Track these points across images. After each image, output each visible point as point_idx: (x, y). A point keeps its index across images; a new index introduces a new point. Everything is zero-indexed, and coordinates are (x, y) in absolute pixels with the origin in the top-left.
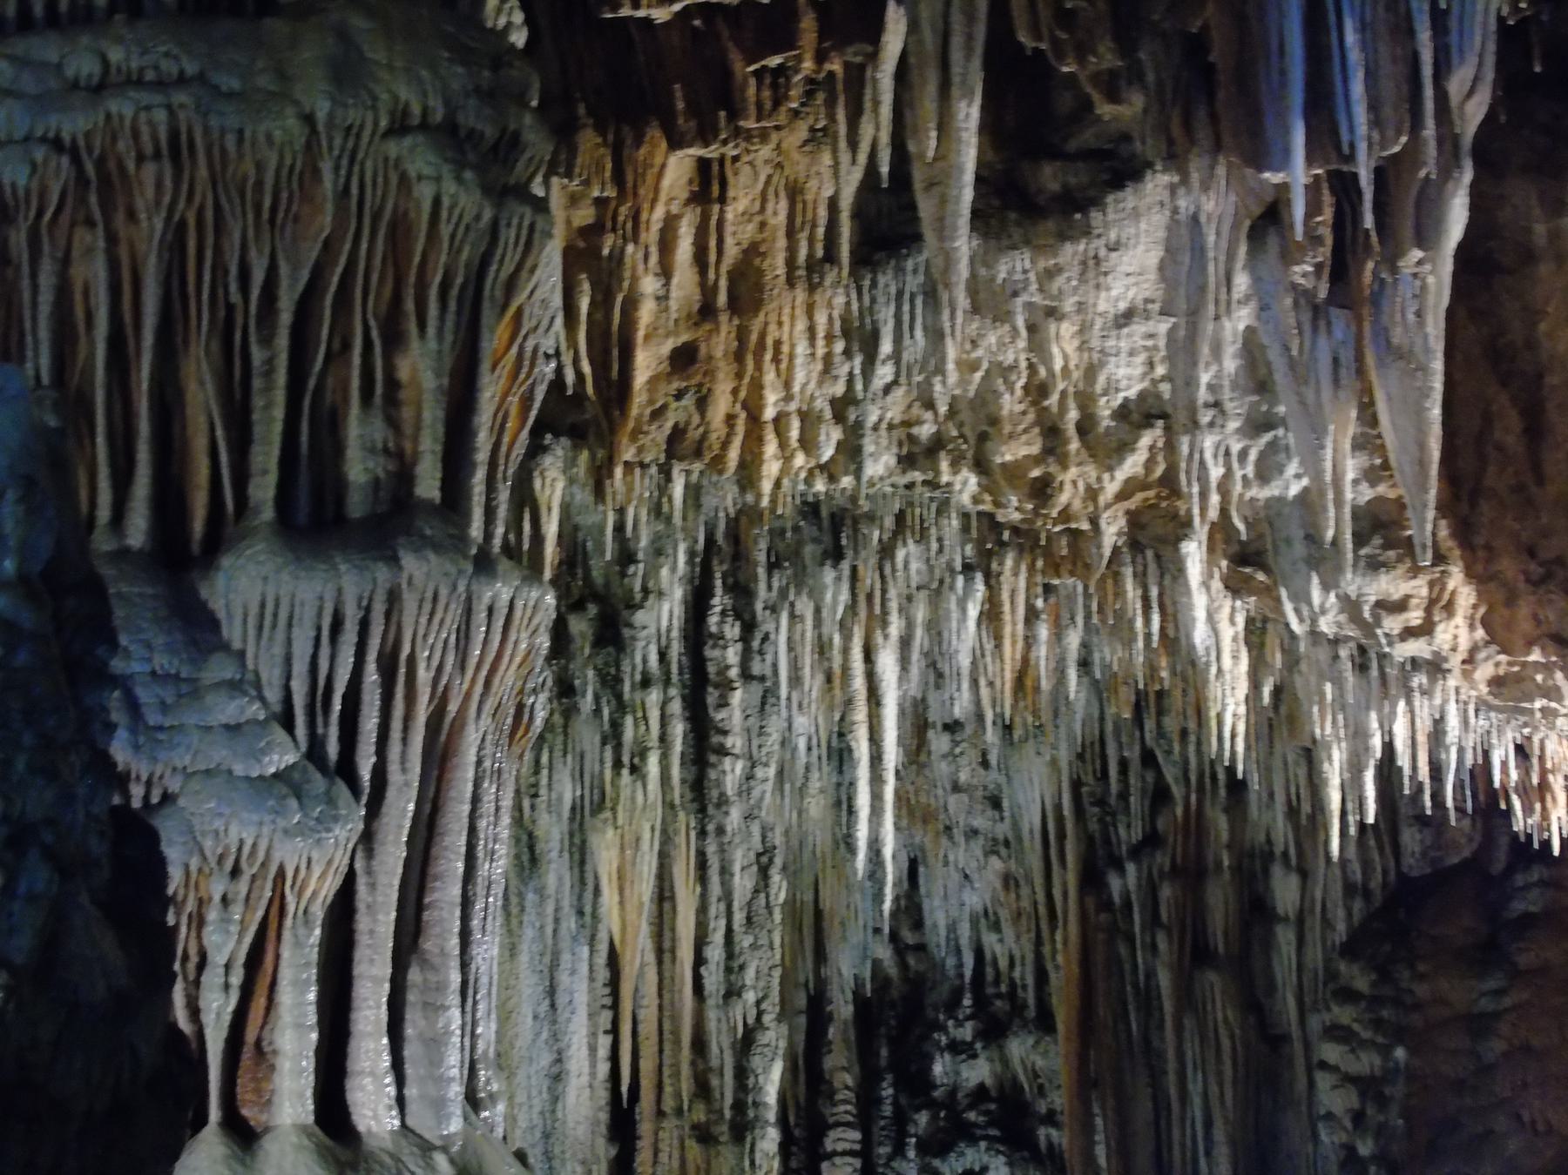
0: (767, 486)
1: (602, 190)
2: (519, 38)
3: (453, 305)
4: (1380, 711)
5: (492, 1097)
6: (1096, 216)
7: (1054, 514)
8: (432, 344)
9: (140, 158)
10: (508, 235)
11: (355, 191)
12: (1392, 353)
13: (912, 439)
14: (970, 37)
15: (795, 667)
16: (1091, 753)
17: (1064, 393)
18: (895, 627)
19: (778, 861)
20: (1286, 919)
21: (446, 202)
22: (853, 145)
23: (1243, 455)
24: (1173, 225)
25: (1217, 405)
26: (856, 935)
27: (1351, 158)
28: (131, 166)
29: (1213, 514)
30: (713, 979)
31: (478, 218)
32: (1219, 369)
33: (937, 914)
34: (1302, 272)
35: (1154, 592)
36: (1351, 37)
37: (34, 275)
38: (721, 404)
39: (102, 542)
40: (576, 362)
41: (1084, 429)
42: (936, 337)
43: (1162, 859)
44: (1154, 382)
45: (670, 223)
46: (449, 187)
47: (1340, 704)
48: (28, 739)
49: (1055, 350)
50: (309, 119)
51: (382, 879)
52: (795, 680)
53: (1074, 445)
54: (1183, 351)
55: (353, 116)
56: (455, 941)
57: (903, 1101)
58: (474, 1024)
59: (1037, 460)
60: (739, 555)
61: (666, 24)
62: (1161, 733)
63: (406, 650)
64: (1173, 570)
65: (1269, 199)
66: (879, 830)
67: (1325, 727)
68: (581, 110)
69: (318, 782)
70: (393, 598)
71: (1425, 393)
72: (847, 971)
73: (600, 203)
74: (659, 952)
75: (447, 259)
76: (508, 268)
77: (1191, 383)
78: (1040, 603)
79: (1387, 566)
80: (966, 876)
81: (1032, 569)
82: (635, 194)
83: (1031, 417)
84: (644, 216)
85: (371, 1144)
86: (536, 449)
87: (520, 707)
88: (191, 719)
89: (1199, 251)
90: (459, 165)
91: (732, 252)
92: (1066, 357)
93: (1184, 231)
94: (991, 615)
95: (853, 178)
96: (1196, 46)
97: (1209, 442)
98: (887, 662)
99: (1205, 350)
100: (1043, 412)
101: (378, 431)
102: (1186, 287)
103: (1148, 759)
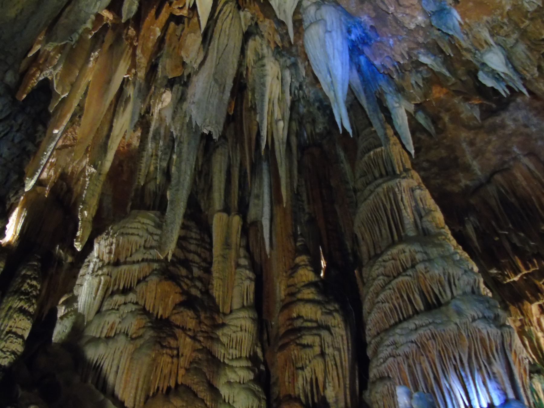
1: (369, 157)
3: (500, 353)
9: (427, 340)
10: (505, 335)
11: (470, 335)
21: (489, 332)
31: (498, 333)
46: (489, 329)
50: (456, 324)
61: (518, 281)
68: (508, 302)
73: (521, 320)
76: (509, 341)
82: (527, 316)
84: (532, 320)
86: (531, 378)
90: (489, 324)
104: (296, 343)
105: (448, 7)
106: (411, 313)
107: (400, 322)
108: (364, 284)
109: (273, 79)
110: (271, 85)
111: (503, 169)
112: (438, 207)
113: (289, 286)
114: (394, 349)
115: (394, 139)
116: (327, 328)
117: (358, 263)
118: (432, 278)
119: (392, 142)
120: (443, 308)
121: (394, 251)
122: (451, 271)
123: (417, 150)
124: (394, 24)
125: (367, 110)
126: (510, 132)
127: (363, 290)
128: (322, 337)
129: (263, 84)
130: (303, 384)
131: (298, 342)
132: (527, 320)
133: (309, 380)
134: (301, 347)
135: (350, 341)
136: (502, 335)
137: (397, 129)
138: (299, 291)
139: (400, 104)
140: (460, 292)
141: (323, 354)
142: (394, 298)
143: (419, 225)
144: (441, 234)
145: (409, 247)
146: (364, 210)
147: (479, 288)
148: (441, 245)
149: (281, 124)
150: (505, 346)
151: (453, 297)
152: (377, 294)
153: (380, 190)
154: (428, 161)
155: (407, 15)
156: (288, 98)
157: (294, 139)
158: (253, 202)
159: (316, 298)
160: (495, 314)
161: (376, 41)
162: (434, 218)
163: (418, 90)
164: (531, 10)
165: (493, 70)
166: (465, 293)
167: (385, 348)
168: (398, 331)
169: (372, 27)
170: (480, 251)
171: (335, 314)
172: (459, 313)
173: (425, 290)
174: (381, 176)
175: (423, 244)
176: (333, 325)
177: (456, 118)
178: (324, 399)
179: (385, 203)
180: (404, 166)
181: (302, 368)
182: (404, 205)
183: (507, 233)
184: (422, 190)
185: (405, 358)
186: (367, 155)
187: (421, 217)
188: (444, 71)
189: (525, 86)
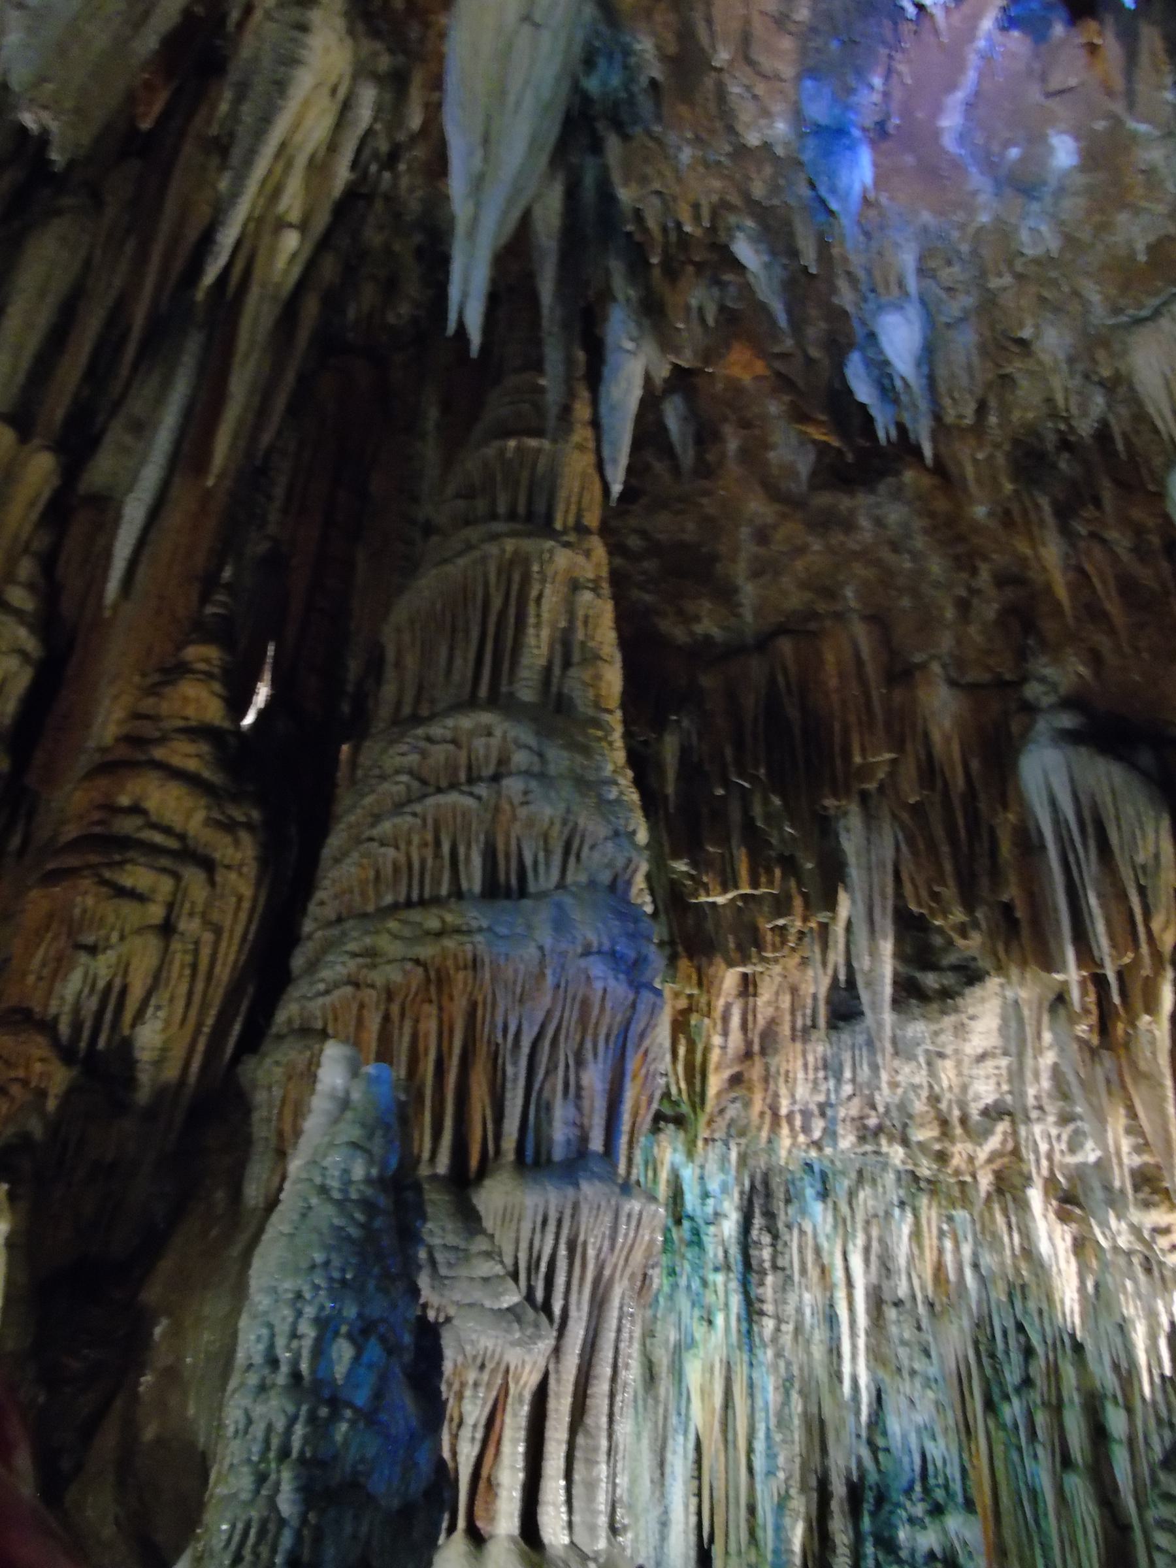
0: (783, 1153)
1: (502, 452)
2: (649, 909)
3: (611, 1045)
4: (1163, 1299)
5: (625, 1528)
6: (960, 1001)
7: (950, 1171)
8: (601, 1066)
9: (458, 969)
10: (641, 1007)
12: (1141, 1076)
13: (865, 1127)
14: (884, 908)
15: (803, 1263)
16: (982, 1323)
17: (950, 1101)
18: (860, 1240)
19: (797, 1385)
20: (1121, 1442)
22: (824, 964)
23: (1059, 1137)
24: (1004, 1006)
25: (1040, 1108)
26: (848, 1438)
27: (1102, 966)
28: (452, 972)
29: (1045, 1172)
30: (759, 1463)
32: (1038, 1087)
33: (894, 1425)
34: (1082, 1029)
35: (1013, 1219)
36: (1093, 901)
37: (401, 1028)
38: (758, 1105)
39: (424, 1171)
40: (678, 1083)
41: (964, 1120)
42: (875, 1068)
43: (1035, 1396)
44: (1002, 1094)
45: (728, 1007)
46: (612, 983)
47: (1138, 1295)
48: (376, 1270)
49: (943, 1076)
50: (541, 948)
51: (564, 1377)
52: (803, 1271)
53: (958, 1131)
54: (1016, 1076)
55: (563, 946)
56: (604, 1420)
57: (881, 1557)
58: (615, 1475)
59: (938, 1140)
60: (768, 1195)
62: (1025, 1312)
63: (581, 1238)
64: (1023, 1205)
65: (1057, 989)
66: (857, 1368)
67: (1130, 1309)
69: (530, 1313)
70: (576, 1207)
71: (1163, 1099)
72: (841, 1463)
73: (690, 996)
74: (726, 1441)
75: (608, 1021)
76: (642, 1025)
77: (1022, 1094)
78: (945, 1227)
79: (1155, 1205)
80: (912, 1402)
81: (940, 1205)
82: (708, 992)
83: (967, 301)
85: (551, 1552)
87: (645, 1275)
88: (463, 1272)
89: (1021, 1021)
91: (761, 1021)
92: (949, 1079)
93: (1011, 1010)
94: (916, 1234)
95: (825, 983)
96: (1007, 909)
97: (1037, 1129)
98: (856, 1262)
99: (1029, 1075)
100: (939, 1111)
101: (572, 1112)
102: (1016, 1040)
103: (1020, 1328)
104: (100, 876)
105: (856, 133)
106: (444, 890)
107: (409, 904)
108: (353, 781)
109: (317, 86)
110: (306, 103)
111: (803, 628)
112: (618, 657)
113: (137, 716)
114: (366, 966)
115: (582, 434)
116: (208, 865)
117: (358, 727)
118: (530, 823)
119: (576, 438)
120: (527, 903)
121: (466, 722)
122: (582, 821)
123: (629, 494)
124: (713, 107)
125: (545, 311)
126: (857, 547)
127: (345, 798)
128: (183, 884)
129: (281, 86)
130: (81, 992)
131: (107, 874)
132: (703, 1000)
133: (101, 984)
134: (111, 892)
135: (257, 917)
136: (634, 1006)
137: (603, 409)
138: (163, 740)
139: (638, 346)
140: (583, 878)
141: (167, 929)
142: (416, 839)
143: (555, 680)
144: (597, 723)
145: (506, 725)
146: (427, 588)
147: (629, 883)
148: (585, 750)
149: (291, 241)
150: (630, 1035)
151: (561, 885)
152: (377, 818)
153: (493, 549)
154: (643, 534)
155: (755, 97)
156: (342, 174)
157: (311, 307)
158: (117, 433)
159: (207, 774)
160: (639, 953)
161: (649, 133)
162: (598, 677)
163: (698, 330)
164: (1029, 252)
165: (887, 363)
166: (592, 884)
167: (346, 958)
168: (392, 925)
169: (653, 83)
170: (672, 811)
171: (245, 837)
172: (561, 924)
173: (501, 847)
174: (512, 516)
175: (545, 731)
176: (226, 862)
177: (752, 455)
178: (125, 1047)
179: (492, 590)
180: (579, 516)
181: (93, 950)
182: (538, 616)
183: (746, 785)
184: (599, 596)
185: (384, 996)
186: (497, 444)
187: (567, 664)
188: (778, 307)
189: (934, 439)
